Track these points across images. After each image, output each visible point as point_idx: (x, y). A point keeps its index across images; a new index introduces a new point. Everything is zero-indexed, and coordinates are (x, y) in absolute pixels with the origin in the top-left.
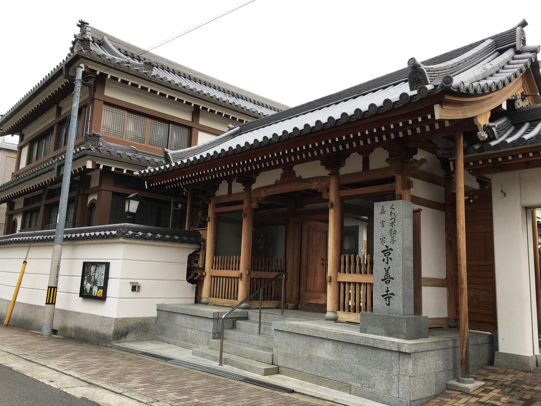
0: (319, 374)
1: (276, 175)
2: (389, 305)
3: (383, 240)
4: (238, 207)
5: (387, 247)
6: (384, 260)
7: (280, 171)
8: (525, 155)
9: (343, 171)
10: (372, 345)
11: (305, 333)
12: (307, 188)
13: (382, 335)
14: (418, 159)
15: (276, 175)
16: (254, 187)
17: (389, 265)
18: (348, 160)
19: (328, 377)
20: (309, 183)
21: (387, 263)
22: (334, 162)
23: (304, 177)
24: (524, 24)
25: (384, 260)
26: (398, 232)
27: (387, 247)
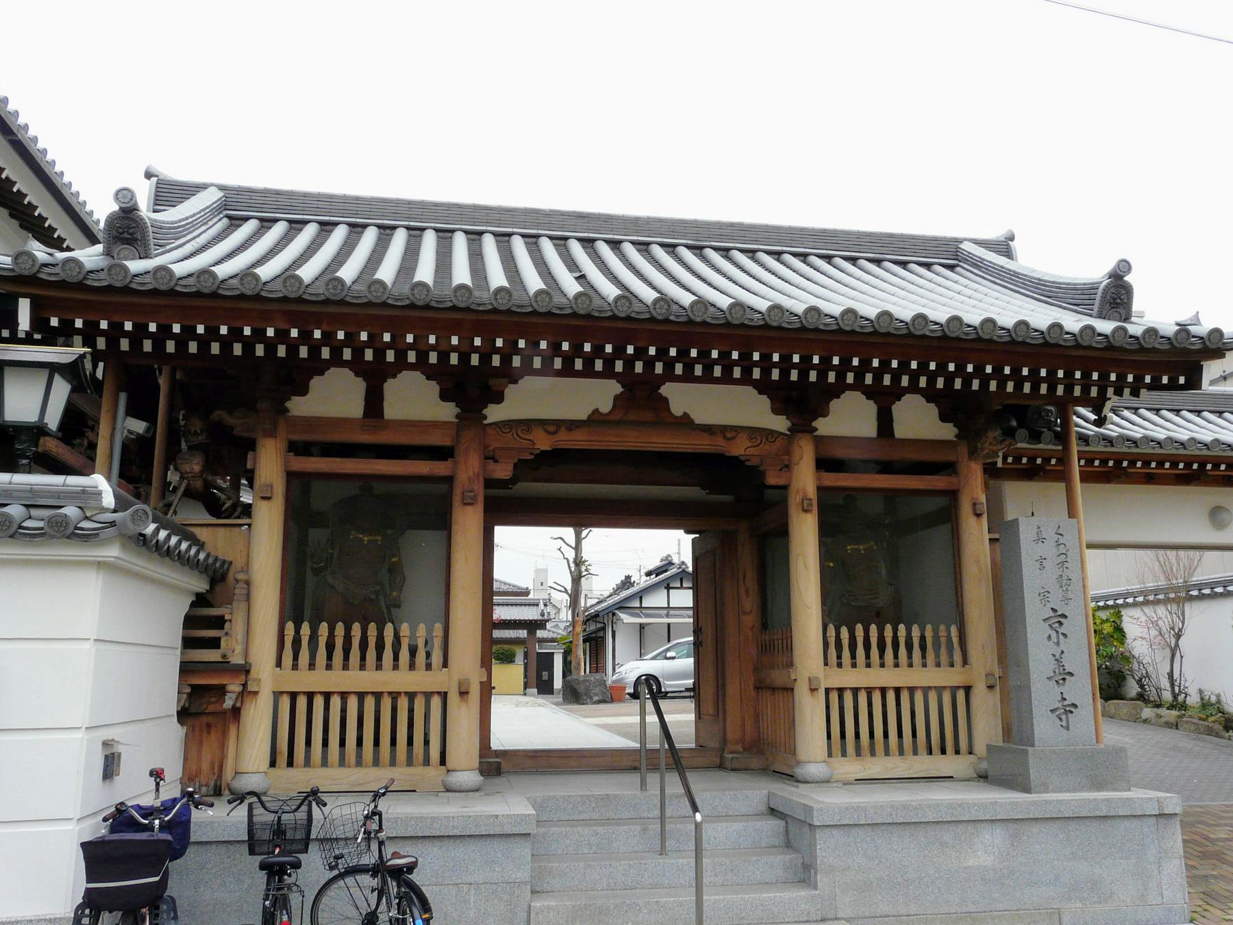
0: (972, 908)
1: (601, 395)
2: (1068, 728)
3: (1044, 595)
4: (439, 468)
5: (1054, 610)
6: (1049, 637)
7: (614, 388)
8: (1146, 464)
9: (824, 426)
10: (1104, 814)
11: (931, 817)
12: (719, 450)
13: (1081, 790)
14: (677, 409)
15: (601, 395)
16: (494, 413)
17: (1062, 647)
18: (834, 404)
19: (1001, 907)
20: (725, 437)
21: (1058, 644)
22: (801, 403)
23: (699, 418)
24: (1012, 238)
25: (1049, 637)
26: (1074, 580)
27: (1054, 610)
